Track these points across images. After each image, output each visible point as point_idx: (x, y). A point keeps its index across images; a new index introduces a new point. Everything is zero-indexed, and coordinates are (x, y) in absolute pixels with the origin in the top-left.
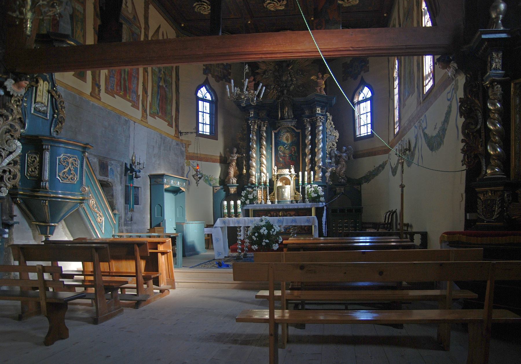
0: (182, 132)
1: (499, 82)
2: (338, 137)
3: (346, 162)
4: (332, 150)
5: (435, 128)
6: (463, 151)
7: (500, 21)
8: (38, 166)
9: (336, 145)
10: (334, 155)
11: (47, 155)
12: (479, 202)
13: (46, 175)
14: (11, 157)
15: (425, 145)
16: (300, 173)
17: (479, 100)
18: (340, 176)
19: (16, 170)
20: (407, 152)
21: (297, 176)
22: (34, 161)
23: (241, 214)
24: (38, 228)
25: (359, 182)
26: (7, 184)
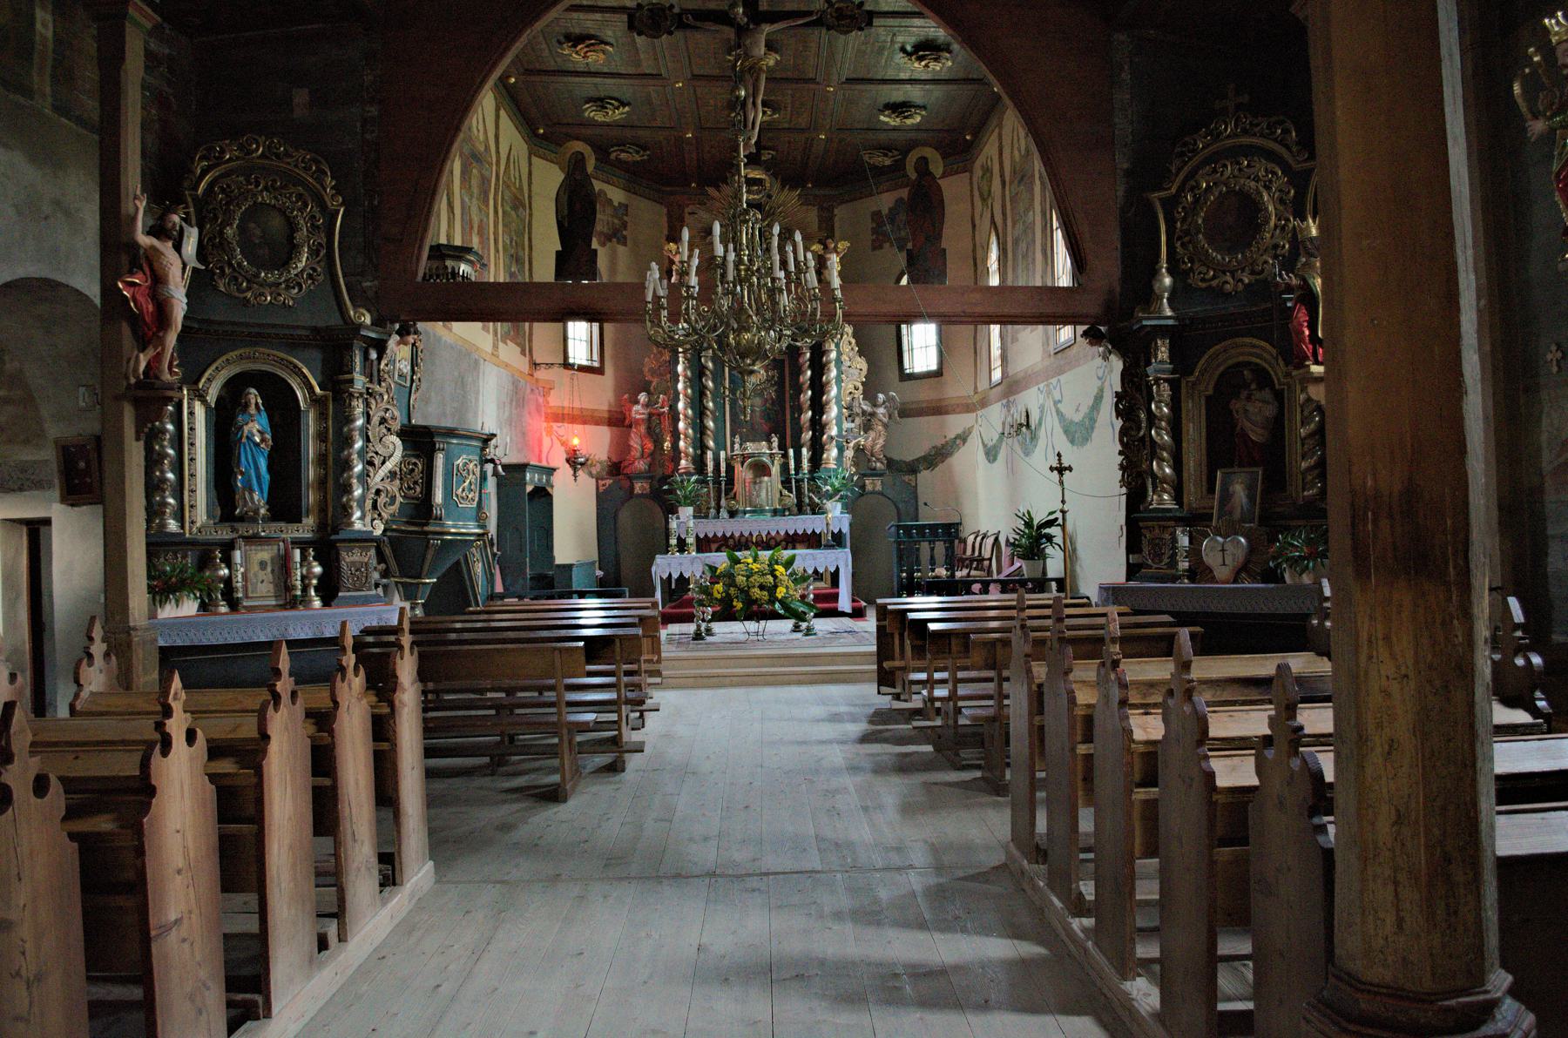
0: (537, 362)
1: (1166, 380)
2: (865, 372)
3: (885, 426)
4: (853, 399)
5: (1077, 410)
6: (1122, 467)
7: (1165, 300)
8: (422, 478)
9: (861, 388)
10: (859, 411)
11: (440, 459)
12: (1144, 542)
13: (438, 497)
14: (389, 465)
15: (1058, 430)
16: (791, 452)
17: (1141, 394)
18: (872, 455)
19: (393, 488)
20: (1024, 429)
21: (785, 456)
22: (413, 470)
23: (694, 548)
24: (401, 589)
25: (913, 468)
26: (383, 514)
